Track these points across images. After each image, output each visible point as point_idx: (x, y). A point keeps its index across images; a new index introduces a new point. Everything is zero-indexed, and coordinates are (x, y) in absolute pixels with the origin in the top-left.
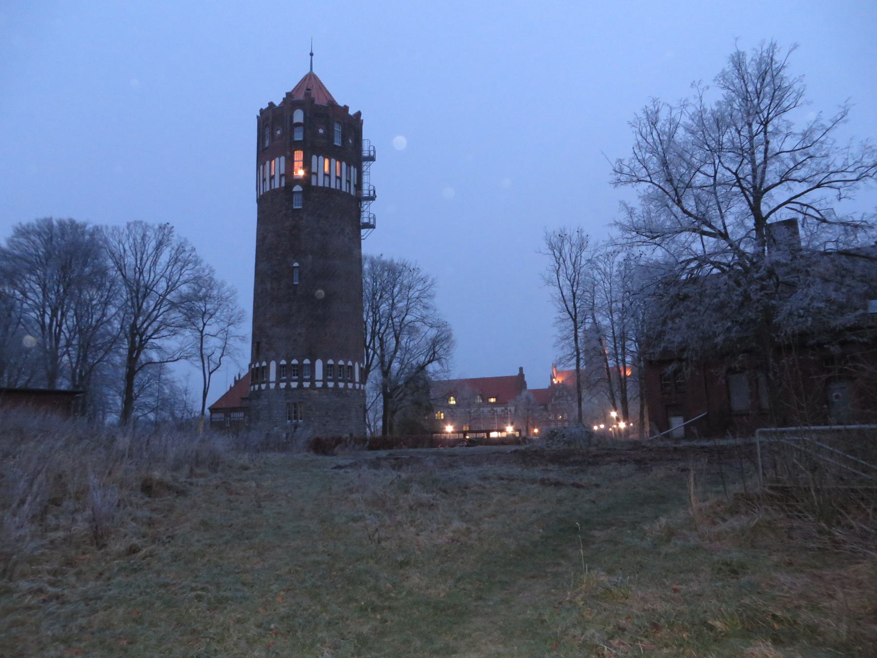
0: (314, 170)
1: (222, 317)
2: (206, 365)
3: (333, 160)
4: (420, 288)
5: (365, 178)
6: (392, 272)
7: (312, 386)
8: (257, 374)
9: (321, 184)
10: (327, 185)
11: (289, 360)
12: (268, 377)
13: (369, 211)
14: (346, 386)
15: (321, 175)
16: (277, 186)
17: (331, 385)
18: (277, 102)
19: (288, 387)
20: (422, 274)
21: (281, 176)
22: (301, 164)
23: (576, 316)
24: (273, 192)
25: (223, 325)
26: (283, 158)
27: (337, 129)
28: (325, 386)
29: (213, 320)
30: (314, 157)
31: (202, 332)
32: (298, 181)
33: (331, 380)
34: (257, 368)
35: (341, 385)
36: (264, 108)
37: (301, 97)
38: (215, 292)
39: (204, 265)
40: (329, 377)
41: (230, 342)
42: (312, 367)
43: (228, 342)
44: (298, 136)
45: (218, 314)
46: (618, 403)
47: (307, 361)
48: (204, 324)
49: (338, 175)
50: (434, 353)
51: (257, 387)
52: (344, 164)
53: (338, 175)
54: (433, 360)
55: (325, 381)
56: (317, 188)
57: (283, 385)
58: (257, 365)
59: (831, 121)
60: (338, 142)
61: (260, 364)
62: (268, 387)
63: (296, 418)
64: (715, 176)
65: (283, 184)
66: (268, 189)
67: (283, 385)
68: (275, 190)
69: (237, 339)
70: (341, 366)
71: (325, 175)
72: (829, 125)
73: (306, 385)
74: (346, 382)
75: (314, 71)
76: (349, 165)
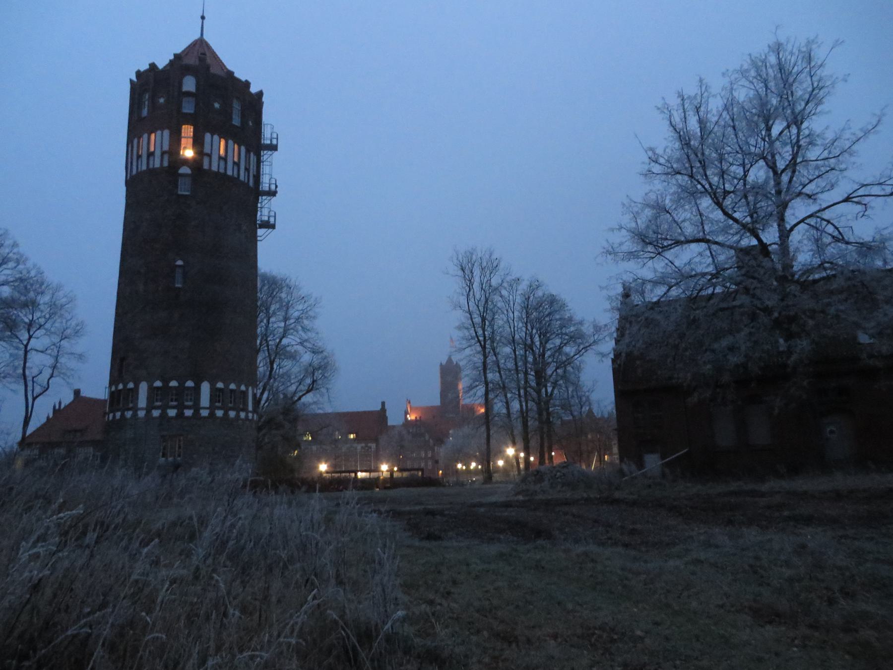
0: (207, 149)
2: (30, 388)
3: (231, 142)
4: (300, 307)
6: (275, 284)
9: (214, 168)
10: (222, 171)
11: (166, 381)
13: (266, 208)
14: (238, 416)
15: (215, 158)
17: (219, 413)
19: (164, 415)
20: (303, 292)
21: (163, 153)
22: (191, 141)
24: (151, 172)
25: (56, 339)
26: (166, 133)
27: (236, 106)
28: (212, 414)
30: (208, 136)
31: (26, 346)
32: (185, 162)
33: (219, 408)
35: (232, 414)
36: (142, 69)
37: (192, 61)
39: (29, 264)
40: (217, 404)
41: (62, 360)
42: (197, 389)
44: (188, 107)
45: (48, 326)
46: (519, 439)
47: (190, 384)
48: (30, 337)
49: (236, 160)
50: (314, 382)
51: (118, 415)
52: (243, 149)
53: (236, 160)
55: (212, 408)
57: (156, 413)
58: (121, 387)
59: (861, 130)
60: (236, 121)
61: (125, 386)
62: (135, 415)
65: (166, 164)
66: (144, 168)
67: (156, 413)
68: (154, 170)
70: (232, 391)
71: (220, 158)
72: (860, 134)
73: (188, 413)
74: (238, 411)
75: (205, 37)
76: (248, 151)
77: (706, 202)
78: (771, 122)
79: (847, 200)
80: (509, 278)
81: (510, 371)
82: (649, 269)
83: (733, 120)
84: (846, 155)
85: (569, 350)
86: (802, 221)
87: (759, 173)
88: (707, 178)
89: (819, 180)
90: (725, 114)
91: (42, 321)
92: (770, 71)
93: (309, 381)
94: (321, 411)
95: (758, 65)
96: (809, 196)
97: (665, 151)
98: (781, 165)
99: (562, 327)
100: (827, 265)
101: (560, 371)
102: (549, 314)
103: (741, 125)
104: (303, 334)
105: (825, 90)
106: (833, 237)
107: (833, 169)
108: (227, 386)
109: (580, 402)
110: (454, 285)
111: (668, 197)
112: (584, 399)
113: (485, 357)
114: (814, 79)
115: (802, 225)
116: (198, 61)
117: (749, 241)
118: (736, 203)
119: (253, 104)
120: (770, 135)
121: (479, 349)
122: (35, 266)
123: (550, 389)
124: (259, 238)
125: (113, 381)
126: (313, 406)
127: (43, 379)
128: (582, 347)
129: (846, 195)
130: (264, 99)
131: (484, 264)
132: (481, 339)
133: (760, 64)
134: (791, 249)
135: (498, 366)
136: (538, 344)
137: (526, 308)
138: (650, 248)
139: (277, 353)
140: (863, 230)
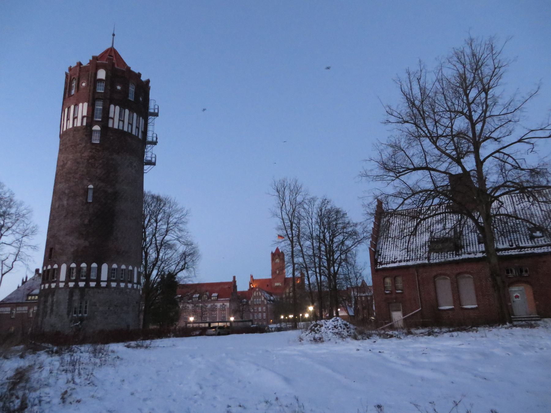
1: (18, 230)
4: (177, 216)
5: (150, 128)
7: (98, 286)
8: (47, 275)
9: (116, 127)
10: (121, 128)
12: (58, 277)
13: (150, 152)
14: (126, 286)
16: (79, 124)
18: (85, 63)
20: (179, 207)
21: (83, 117)
23: (292, 237)
24: (75, 129)
25: (18, 236)
28: (109, 286)
29: (10, 232)
33: (114, 281)
34: (48, 271)
35: (122, 285)
38: (13, 211)
39: (5, 189)
43: (21, 250)
45: (14, 228)
50: (185, 263)
51: (47, 286)
54: (184, 269)
55: (109, 281)
56: (113, 129)
57: (71, 285)
58: (49, 267)
60: (131, 97)
63: (80, 312)
64: (452, 127)
65: (85, 124)
66: (71, 126)
68: (77, 127)
69: (29, 248)
70: (122, 270)
77: (427, 142)
78: (468, 91)
79: (520, 141)
80: (308, 197)
81: (310, 256)
82: (389, 187)
83: (443, 89)
84: (518, 111)
85: (348, 243)
86: (491, 155)
87: (461, 123)
88: (427, 127)
89: (502, 128)
90: (437, 83)
91: (10, 225)
92: (466, 58)
93: (182, 263)
94: (190, 283)
95: (459, 57)
96: (496, 140)
97: (398, 107)
98: (475, 117)
99: (344, 228)
100: (508, 184)
101: (343, 257)
102: (336, 220)
103: (450, 94)
104: (179, 233)
105: (502, 70)
106: (512, 166)
107: (510, 121)
108: (119, 267)
109: (356, 276)
110: (273, 202)
111: (403, 140)
112: (358, 275)
113: (293, 247)
114: (496, 61)
115: (491, 158)
116: (110, 59)
117: (456, 170)
118: (448, 144)
119: (144, 88)
120: (468, 99)
121: (289, 242)
122: (9, 190)
123: (336, 268)
124: (145, 171)
125: (45, 264)
126: (185, 279)
127: (9, 262)
128: (356, 240)
129: (519, 138)
130: (150, 85)
131: (292, 188)
132: (290, 236)
133: (460, 53)
134: (484, 173)
135: (303, 254)
136: (328, 239)
137: (321, 217)
138: (391, 174)
139: (161, 245)
140: (531, 161)
